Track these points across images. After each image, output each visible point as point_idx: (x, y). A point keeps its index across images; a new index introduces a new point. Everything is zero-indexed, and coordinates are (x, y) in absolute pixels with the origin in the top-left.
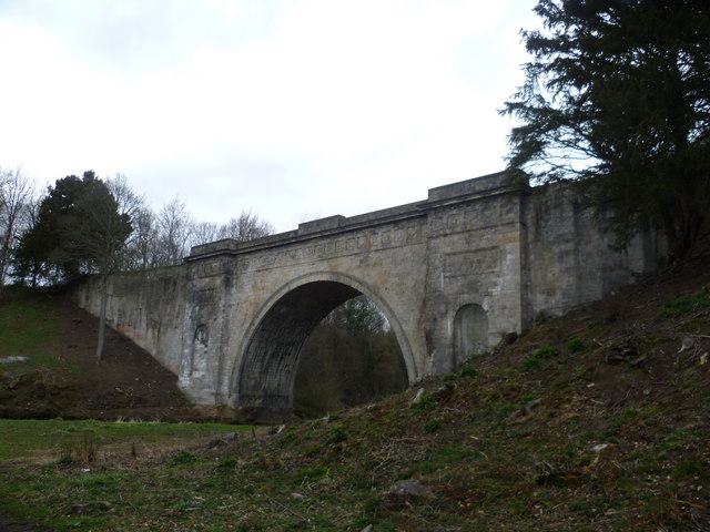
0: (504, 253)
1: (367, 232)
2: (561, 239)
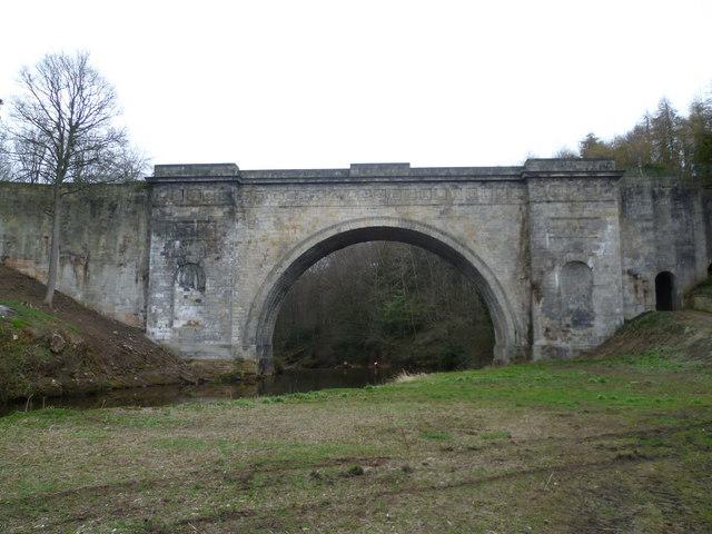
0: (606, 223)
1: (447, 185)
2: (642, 218)
